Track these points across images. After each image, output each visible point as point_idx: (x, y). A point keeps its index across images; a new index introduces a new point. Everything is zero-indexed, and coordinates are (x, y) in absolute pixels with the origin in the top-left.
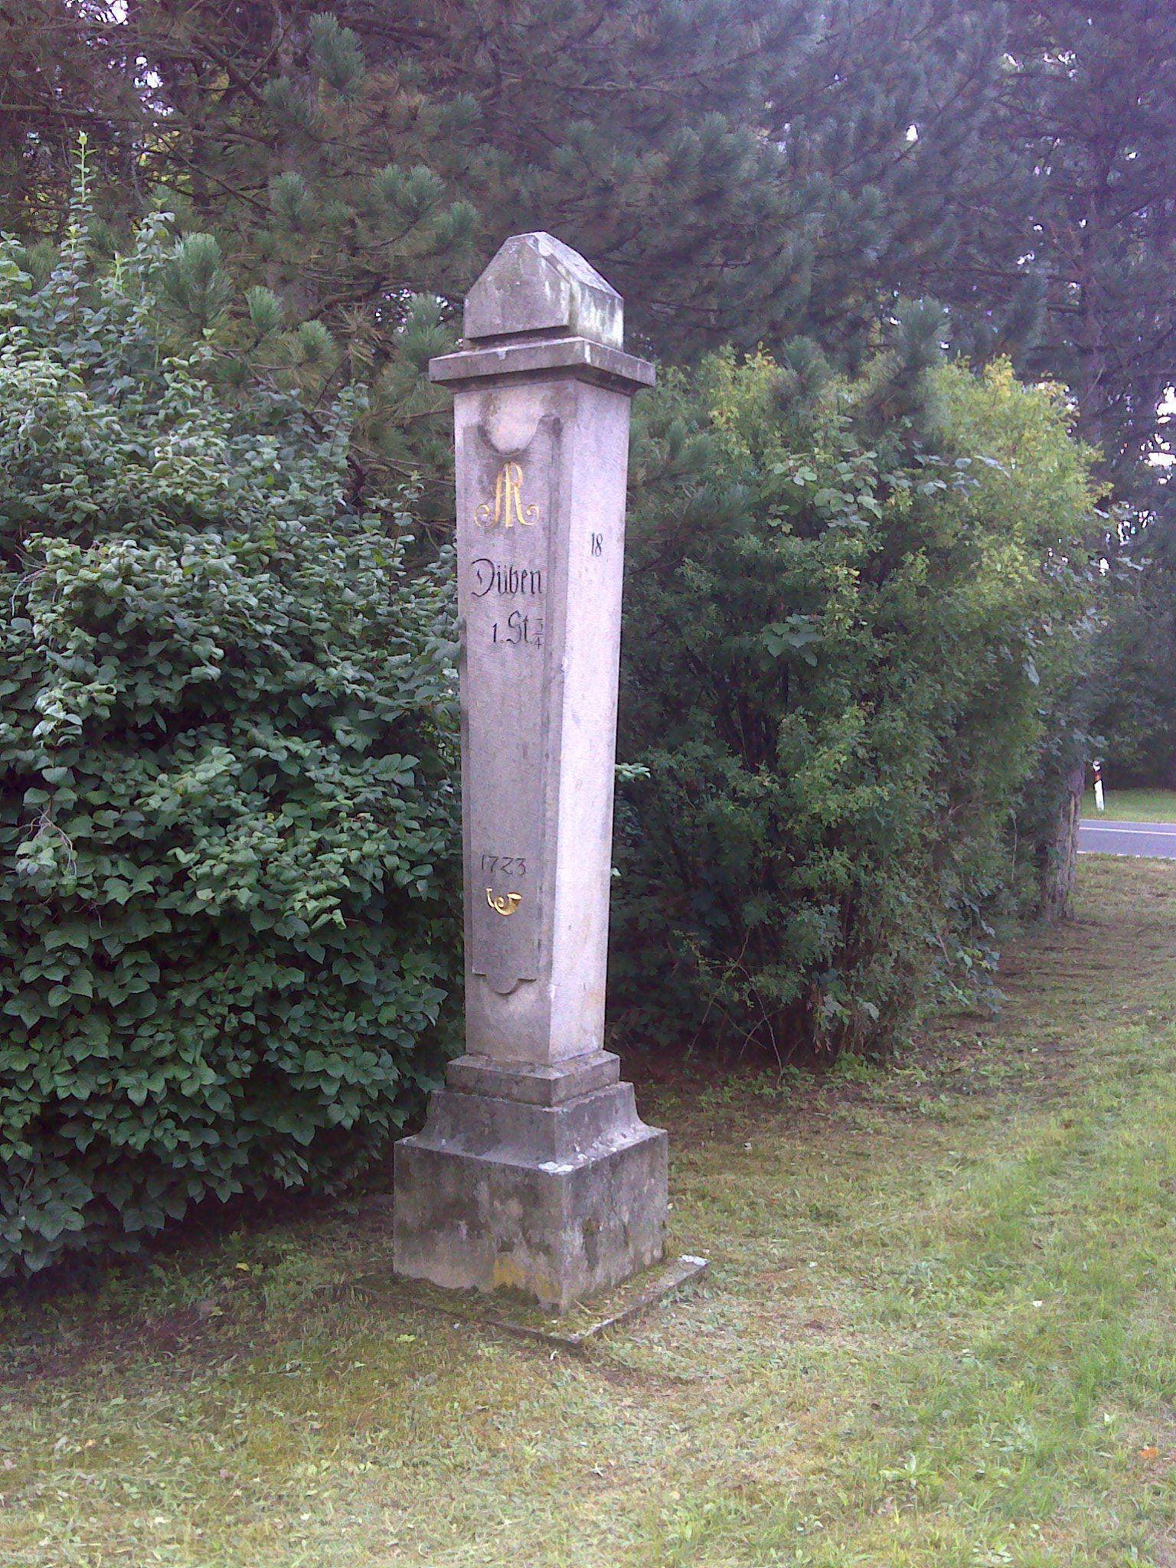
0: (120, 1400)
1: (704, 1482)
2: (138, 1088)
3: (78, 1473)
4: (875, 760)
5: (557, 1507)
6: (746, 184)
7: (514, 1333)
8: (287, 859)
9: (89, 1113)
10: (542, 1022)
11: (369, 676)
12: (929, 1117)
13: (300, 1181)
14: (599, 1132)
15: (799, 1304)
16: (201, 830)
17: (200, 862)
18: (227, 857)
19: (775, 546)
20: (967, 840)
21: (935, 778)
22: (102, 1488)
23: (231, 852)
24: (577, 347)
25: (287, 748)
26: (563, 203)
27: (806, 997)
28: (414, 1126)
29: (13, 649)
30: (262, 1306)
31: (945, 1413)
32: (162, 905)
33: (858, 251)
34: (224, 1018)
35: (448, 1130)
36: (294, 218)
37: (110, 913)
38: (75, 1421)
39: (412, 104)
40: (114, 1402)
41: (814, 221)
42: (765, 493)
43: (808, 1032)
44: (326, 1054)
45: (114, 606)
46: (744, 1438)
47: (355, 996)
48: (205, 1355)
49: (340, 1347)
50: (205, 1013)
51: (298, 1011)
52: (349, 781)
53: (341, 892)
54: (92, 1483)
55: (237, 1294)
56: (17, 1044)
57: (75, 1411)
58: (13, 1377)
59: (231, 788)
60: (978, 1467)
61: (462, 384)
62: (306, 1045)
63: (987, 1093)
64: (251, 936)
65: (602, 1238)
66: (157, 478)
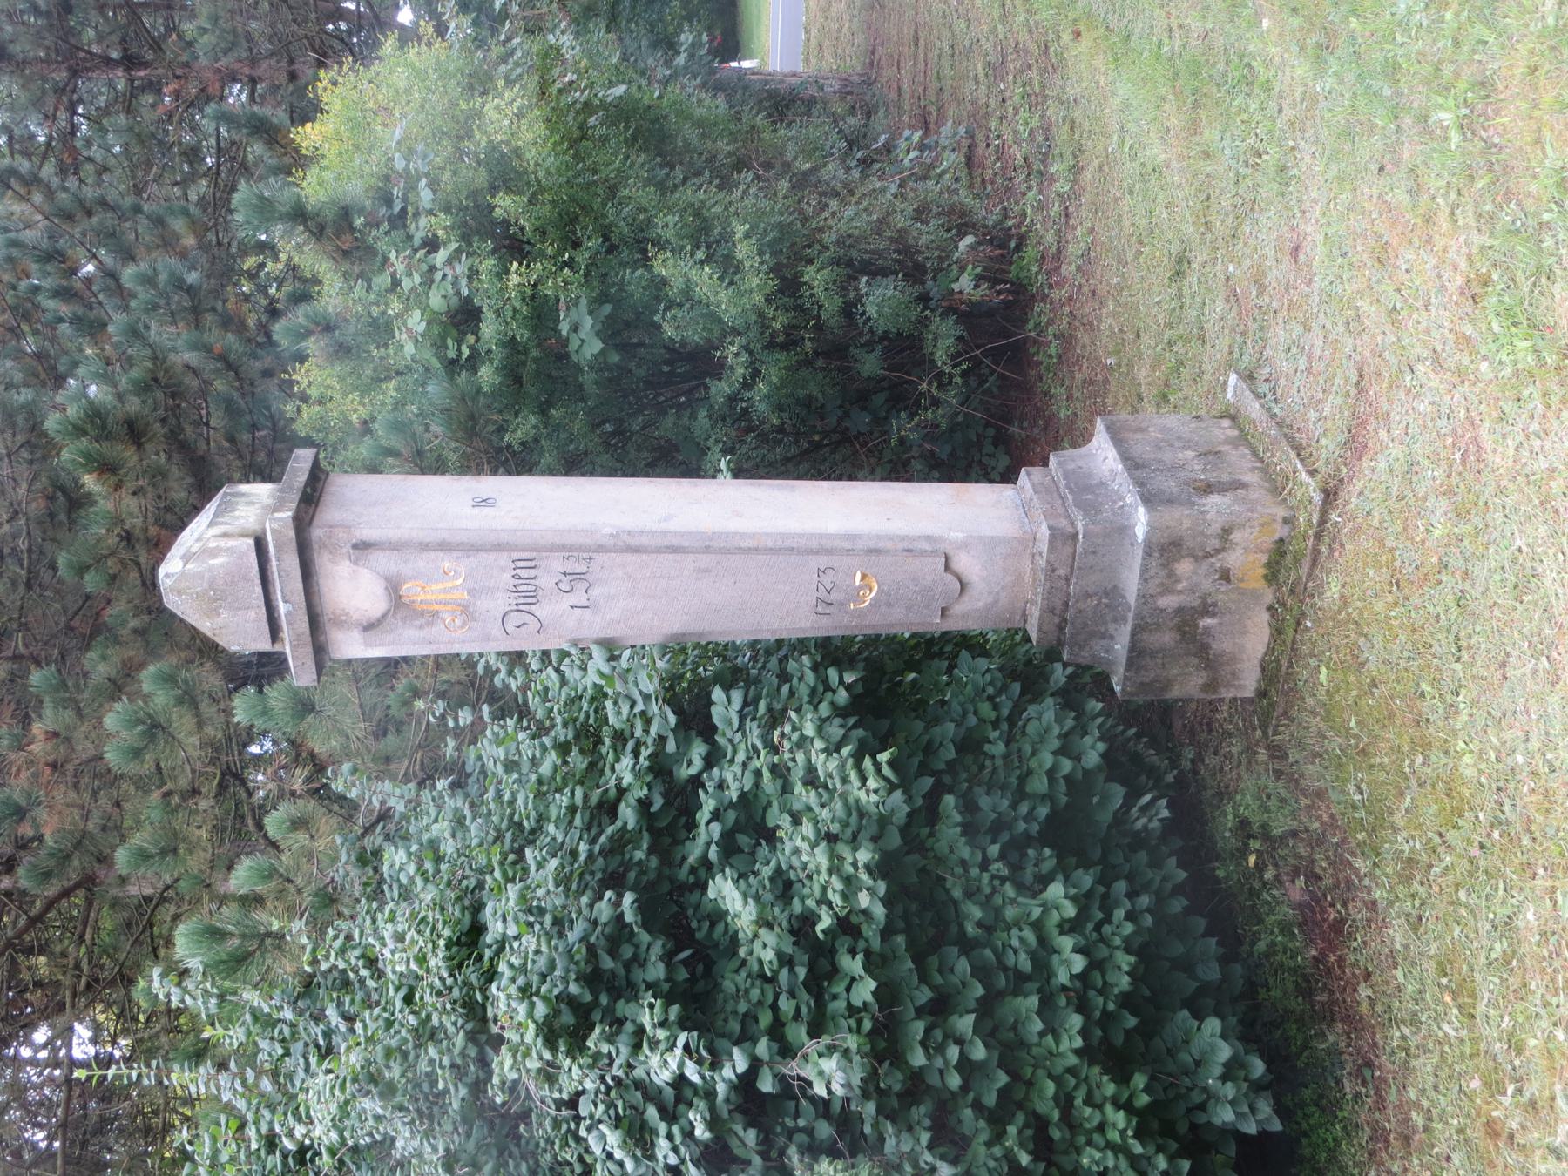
0: (1399, 973)
1: (1468, 339)
2: (1070, 963)
3: (1481, 1007)
4: (706, 238)
5: (1501, 491)
6: (120, 397)
7: (1314, 562)
8: (825, 814)
9: (1098, 1014)
10: (990, 544)
11: (630, 744)
12: (1074, 182)
13: (1164, 802)
14: (1102, 484)
15: (1272, 277)
16: (797, 907)
17: (830, 905)
18: (824, 876)
19: (489, 351)
20: (789, 156)
21: (725, 184)
22: (1497, 980)
23: (819, 873)
24: (276, 526)
25: (708, 824)
26: (144, 584)
27: (955, 311)
28: (1101, 682)
29: (612, 1112)
30: (1294, 834)
31: (1387, 92)
32: (876, 944)
33: (190, 290)
34: (993, 877)
35: (1104, 642)
36: (163, 853)
37: (887, 995)
38: (1423, 1019)
39: (42, 737)
40: (1401, 979)
41: (160, 332)
42: (435, 363)
43: (991, 313)
44: (1030, 772)
45: (563, 1006)
46: (1419, 304)
47: (970, 745)
48: (1347, 888)
49: (1335, 743)
50: (989, 897)
51: (985, 802)
52: (741, 756)
53: (858, 758)
54: (1491, 992)
55: (1281, 863)
56: (1027, 1093)
57: (1415, 1022)
58: (1378, 1092)
59: (751, 878)
60: (1445, 47)
61: (319, 650)
62: (1021, 794)
63: (1047, 129)
64: (908, 853)
65: (1212, 477)
66: (428, 971)
